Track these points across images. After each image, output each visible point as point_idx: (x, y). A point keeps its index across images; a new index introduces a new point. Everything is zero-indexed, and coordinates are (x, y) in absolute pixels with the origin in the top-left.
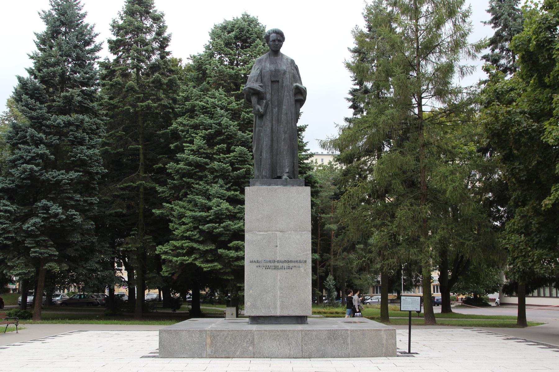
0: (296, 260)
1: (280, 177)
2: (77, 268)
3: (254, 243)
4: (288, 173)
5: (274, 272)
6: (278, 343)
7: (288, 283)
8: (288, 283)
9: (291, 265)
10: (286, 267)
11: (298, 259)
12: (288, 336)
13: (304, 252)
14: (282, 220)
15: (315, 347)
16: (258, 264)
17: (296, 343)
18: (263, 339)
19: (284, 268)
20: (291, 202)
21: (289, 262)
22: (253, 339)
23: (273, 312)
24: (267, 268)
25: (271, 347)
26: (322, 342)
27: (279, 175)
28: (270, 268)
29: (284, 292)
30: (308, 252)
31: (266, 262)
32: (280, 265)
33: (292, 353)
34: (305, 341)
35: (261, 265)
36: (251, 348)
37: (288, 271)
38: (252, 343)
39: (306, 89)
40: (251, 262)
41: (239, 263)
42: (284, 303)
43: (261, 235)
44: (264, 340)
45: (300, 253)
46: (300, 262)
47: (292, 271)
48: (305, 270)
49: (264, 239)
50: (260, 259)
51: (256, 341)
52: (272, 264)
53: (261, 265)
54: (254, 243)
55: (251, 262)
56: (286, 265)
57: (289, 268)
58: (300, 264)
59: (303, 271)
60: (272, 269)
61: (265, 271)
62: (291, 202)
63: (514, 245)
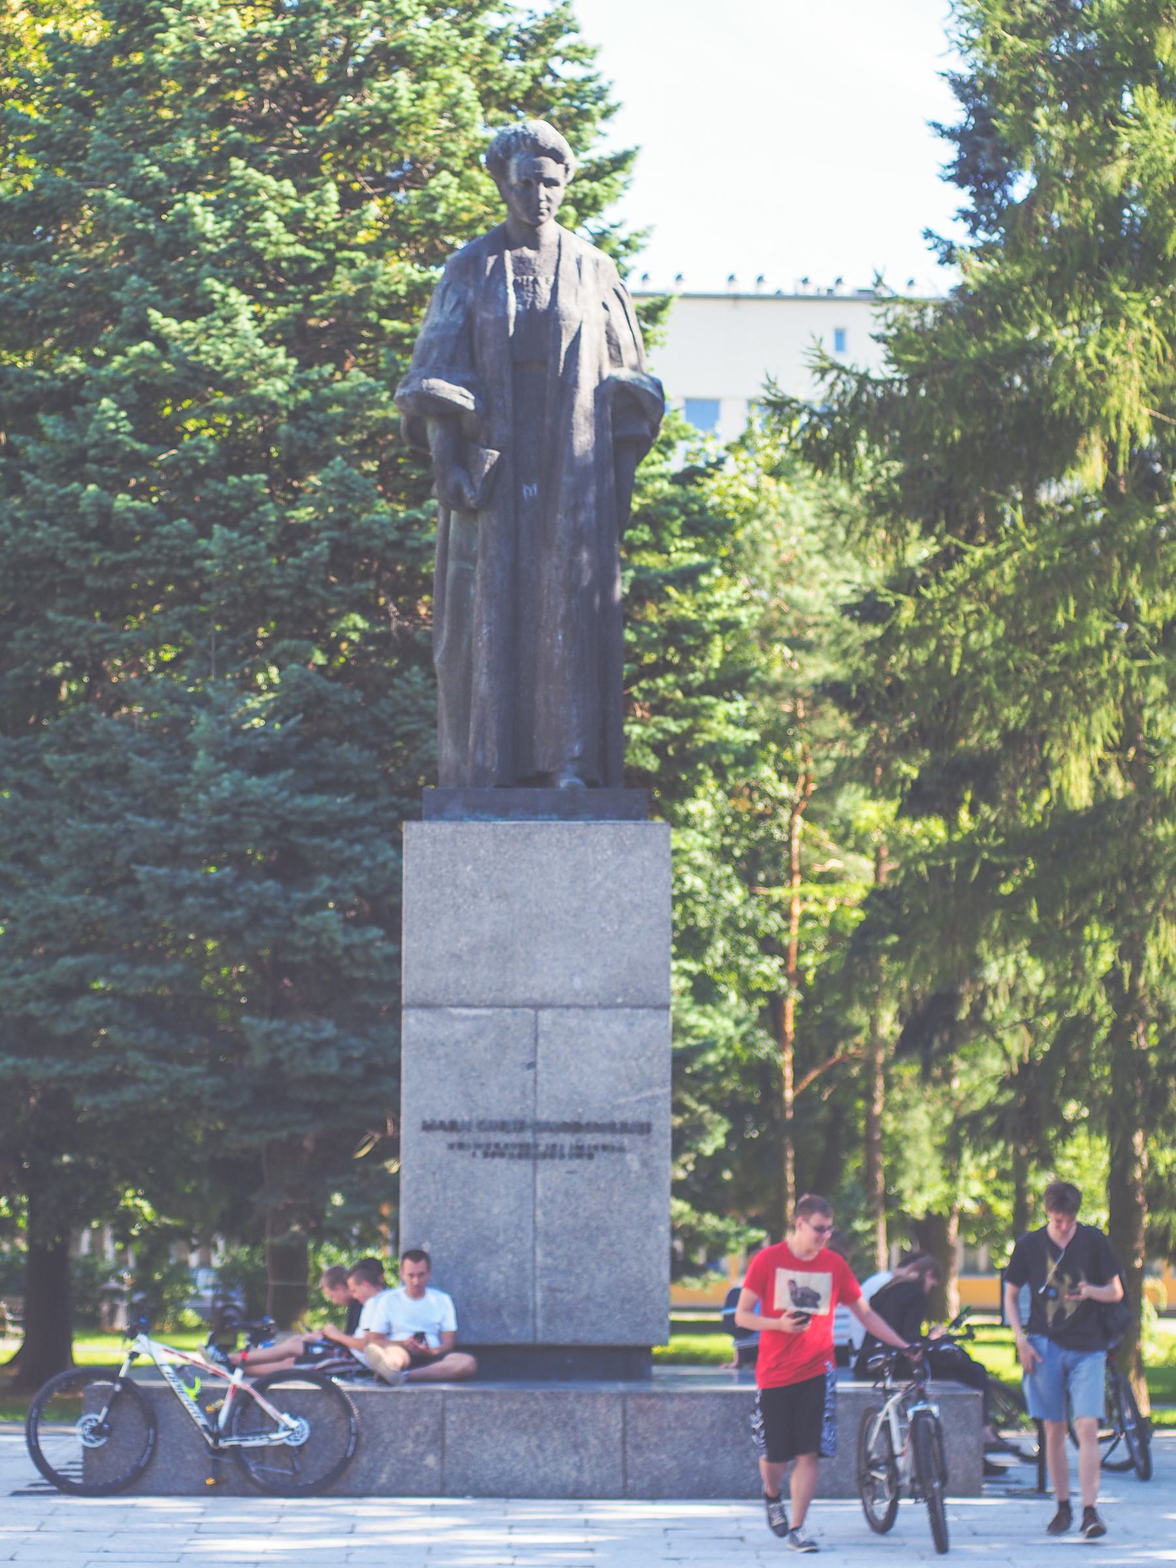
0: (607, 1120)
1: (544, 780)
2: (186, 378)
3: (440, 1051)
4: (578, 759)
5: (522, 1168)
6: (534, 1442)
7: (575, 1215)
8: (575, 1215)
9: (589, 1139)
10: (566, 1150)
11: (618, 1117)
12: (571, 1414)
13: (640, 1090)
14: (556, 959)
15: (674, 1457)
16: (454, 1138)
17: (603, 1443)
18: (477, 1427)
19: (553, 1152)
20: (591, 885)
21: (575, 1127)
22: (442, 1426)
23: (514, 1331)
24: (493, 1152)
25: (508, 1457)
26: (699, 1440)
27: (542, 765)
28: (502, 1155)
29: (559, 1252)
30: (658, 1091)
31: (486, 1126)
32: (546, 1139)
33: (586, 1478)
34: (636, 1434)
35: (467, 1138)
36: (431, 1460)
37: (575, 1164)
38: (438, 1440)
39: (659, 386)
40: (428, 1127)
41: (869, 1253)
42: (559, 1295)
43: (466, 1018)
44: (481, 1432)
45: (625, 1094)
46: (625, 1128)
47: (592, 1166)
48: (645, 1163)
49: (480, 1033)
50: (463, 1116)
51: (451, 1435)
52: (512, 1138)
53: (467, 1138)
54: (440, 1051)
55: (428, 1127)
56: (567, 1140)
57: (580, 1152)
58: (626, 1140)
59: (635, 1165)
60: (512, 1156)
61: (482, 1166)
62: (591, 885)
63: (974, 1065)
